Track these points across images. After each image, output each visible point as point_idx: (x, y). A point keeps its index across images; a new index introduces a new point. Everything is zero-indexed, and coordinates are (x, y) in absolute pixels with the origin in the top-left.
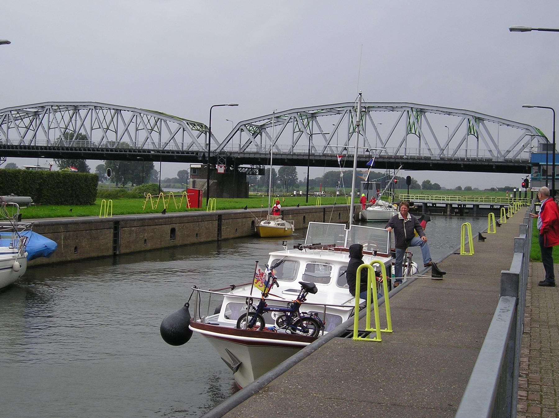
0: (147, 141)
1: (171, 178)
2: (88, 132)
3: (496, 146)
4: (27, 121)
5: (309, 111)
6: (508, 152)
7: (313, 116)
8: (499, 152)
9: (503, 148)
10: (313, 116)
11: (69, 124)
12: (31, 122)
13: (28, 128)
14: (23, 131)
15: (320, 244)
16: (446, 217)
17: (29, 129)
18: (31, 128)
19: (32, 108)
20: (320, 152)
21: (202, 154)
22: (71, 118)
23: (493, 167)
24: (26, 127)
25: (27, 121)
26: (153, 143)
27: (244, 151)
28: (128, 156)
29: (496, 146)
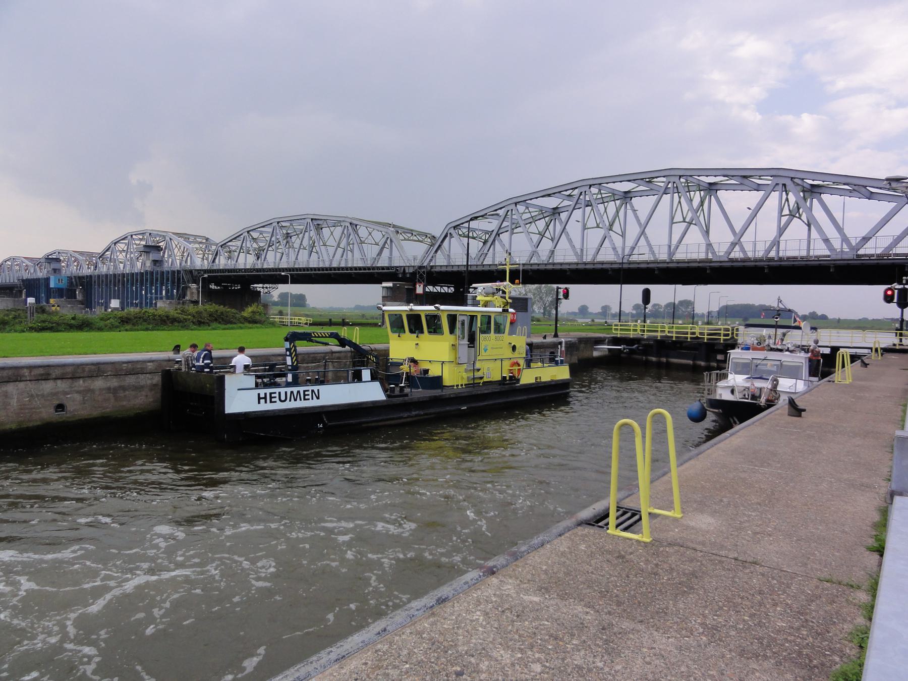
0: (682, 243)
1: (757, 304)
2: (504, 242)
3: (840, 229)
4: (541, 224)
5: (699, 176)
6: (866, 239)
7: (712, 188)
8: (845, 239)
9: (855, 233)
10: (712, 188)
11: (756, 215)
12: (548, 226)
13: (542, 235)
14: (536, 238)
15: (452, 345)
16: (894, 347)
17: (543, 236)
18: (547, 234)
19: (261, 227)
20: (722, 254)
21: (403, 268)
22: (617, 212)
23: (905, 269)
24: (539, 233)
25: (541, 224)
26: (614, 249)
27: (483, 262)
28: (610, 273)
29: (840, 229)
